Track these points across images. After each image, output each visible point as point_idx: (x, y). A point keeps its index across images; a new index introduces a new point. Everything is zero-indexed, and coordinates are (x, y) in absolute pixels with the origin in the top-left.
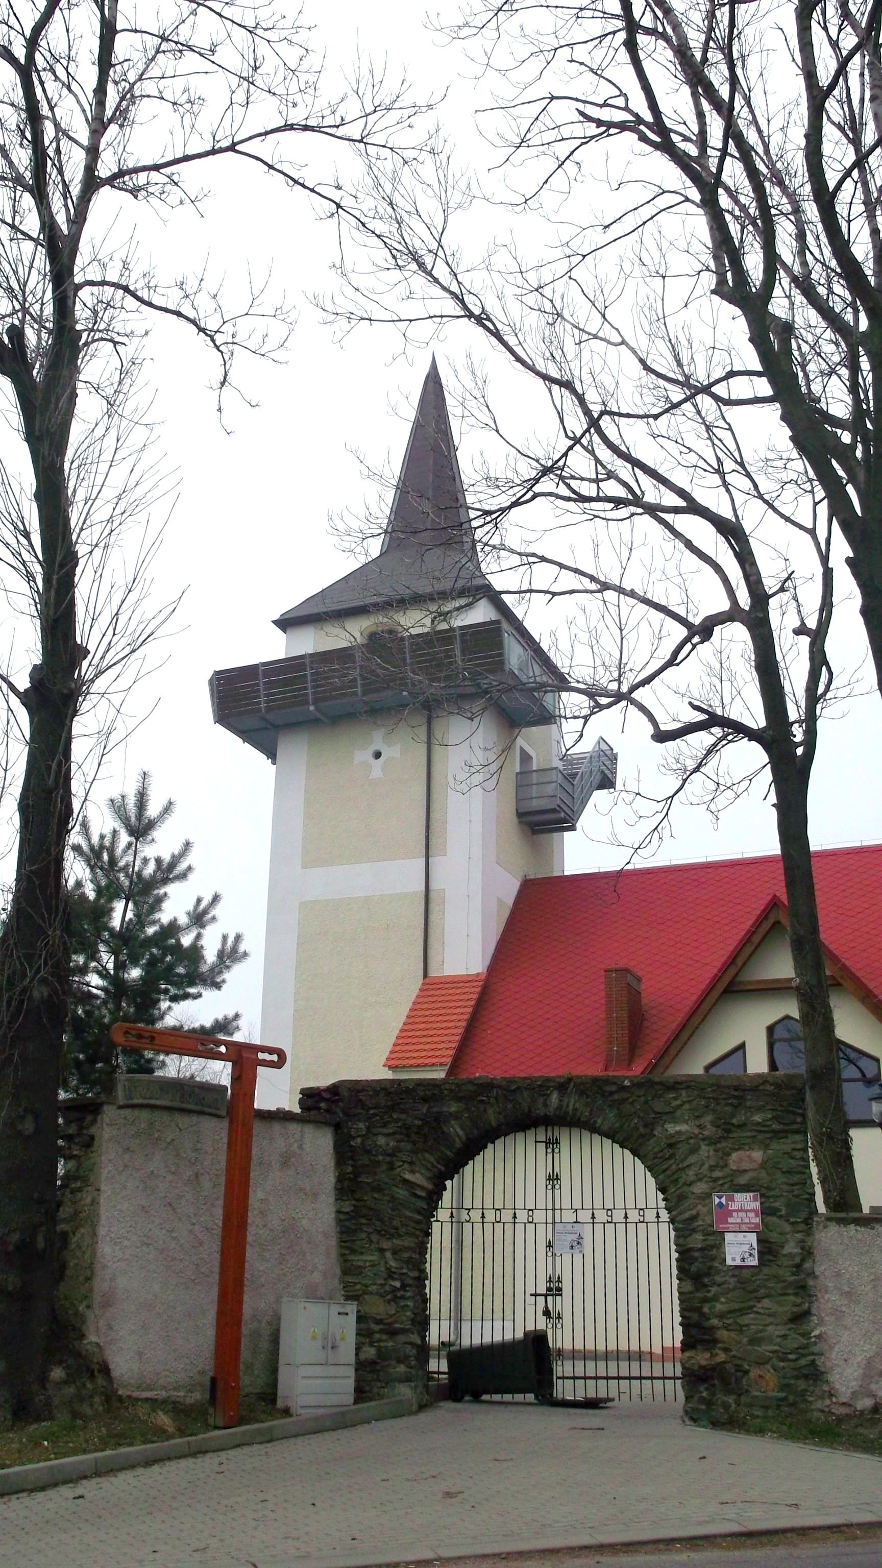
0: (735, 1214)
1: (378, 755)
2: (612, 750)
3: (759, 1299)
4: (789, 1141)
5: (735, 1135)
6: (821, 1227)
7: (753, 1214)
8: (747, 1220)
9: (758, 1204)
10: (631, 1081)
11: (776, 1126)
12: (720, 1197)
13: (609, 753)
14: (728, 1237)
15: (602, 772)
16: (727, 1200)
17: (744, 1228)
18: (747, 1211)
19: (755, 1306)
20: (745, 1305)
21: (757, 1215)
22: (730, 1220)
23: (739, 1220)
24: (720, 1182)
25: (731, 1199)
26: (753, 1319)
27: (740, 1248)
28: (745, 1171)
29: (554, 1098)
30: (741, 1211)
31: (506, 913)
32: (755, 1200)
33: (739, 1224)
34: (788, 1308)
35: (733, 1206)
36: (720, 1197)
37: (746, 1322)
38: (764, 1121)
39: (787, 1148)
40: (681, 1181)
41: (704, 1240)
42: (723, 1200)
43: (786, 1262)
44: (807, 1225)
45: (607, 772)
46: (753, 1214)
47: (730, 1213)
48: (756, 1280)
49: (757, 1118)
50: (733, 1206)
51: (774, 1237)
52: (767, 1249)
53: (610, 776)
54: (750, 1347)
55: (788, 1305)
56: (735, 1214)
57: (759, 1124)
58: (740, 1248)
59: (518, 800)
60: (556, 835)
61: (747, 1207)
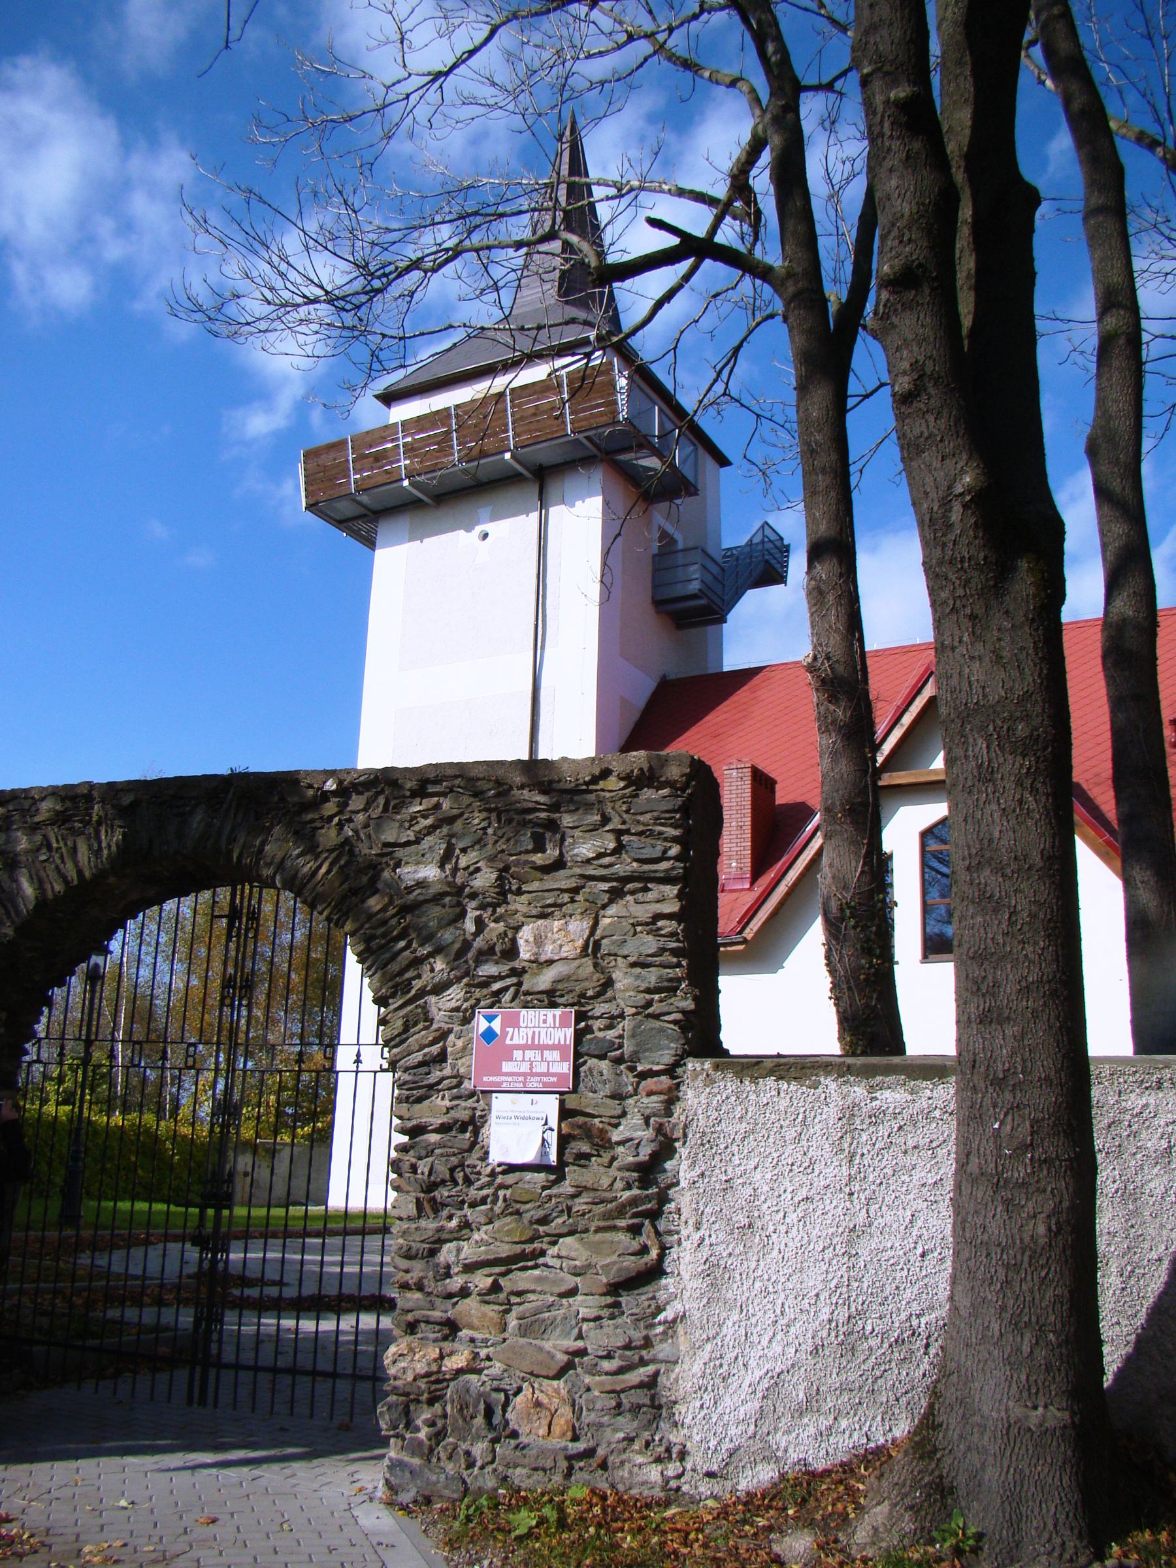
0: (517, 1054)
1: (485, 536)
2: (782, 539)
3: (555, 1239)
4: (650, 896)
5: (535, 885)
6: (699, 1082)
7: (556, 1055)
8: (541, 1068)
9: (570, 1032)
10: (340, 783)
11: (625, 866)
12: (490, 1018)
13: (778, 543)
14: (500, 1103)
15: (767, 561)
16: (503, 1027)
17: (534, 1084)
18: (543, 1048)
19: (543, 1253)
20: (529, 1248)
21: (563, 1059)
22: (507, 1067)
23: (525, 1068)
24: (496, 986)
25: (513, 1022)
26: (540, 1279)
27: (518, 1131)
28: (550, 962)
29: (197, 820)
30: (532, 1047)
31: (636, 716)
32: (564, 1024)
33: (524, 1075)
34: (614, 1258)
35: (516, 1037)
36: (490, 1018)
37: (522, 1286)
38: (600, 856)
39: (643, 913)
40: (417, 984)
41: (448, 1110)
42: (496, 1025)
43: (625, 1156)
44: (673, 1078)
45: (773, 562)
46: (556, 1055)
47: (507, 1053)
48: (550, 1197)
49: (585, 850)
50: (516, 1037)
51: (593, 1100)
52: (579, 1134)
53: (777, 566)
54: (523, 1341)
55: (615, 1253)
56: (517, 1054)
57: (588, 861)
58: (518, 1131)
59: (655, 587)
60: (710, 629)
61: (545, 1040)
